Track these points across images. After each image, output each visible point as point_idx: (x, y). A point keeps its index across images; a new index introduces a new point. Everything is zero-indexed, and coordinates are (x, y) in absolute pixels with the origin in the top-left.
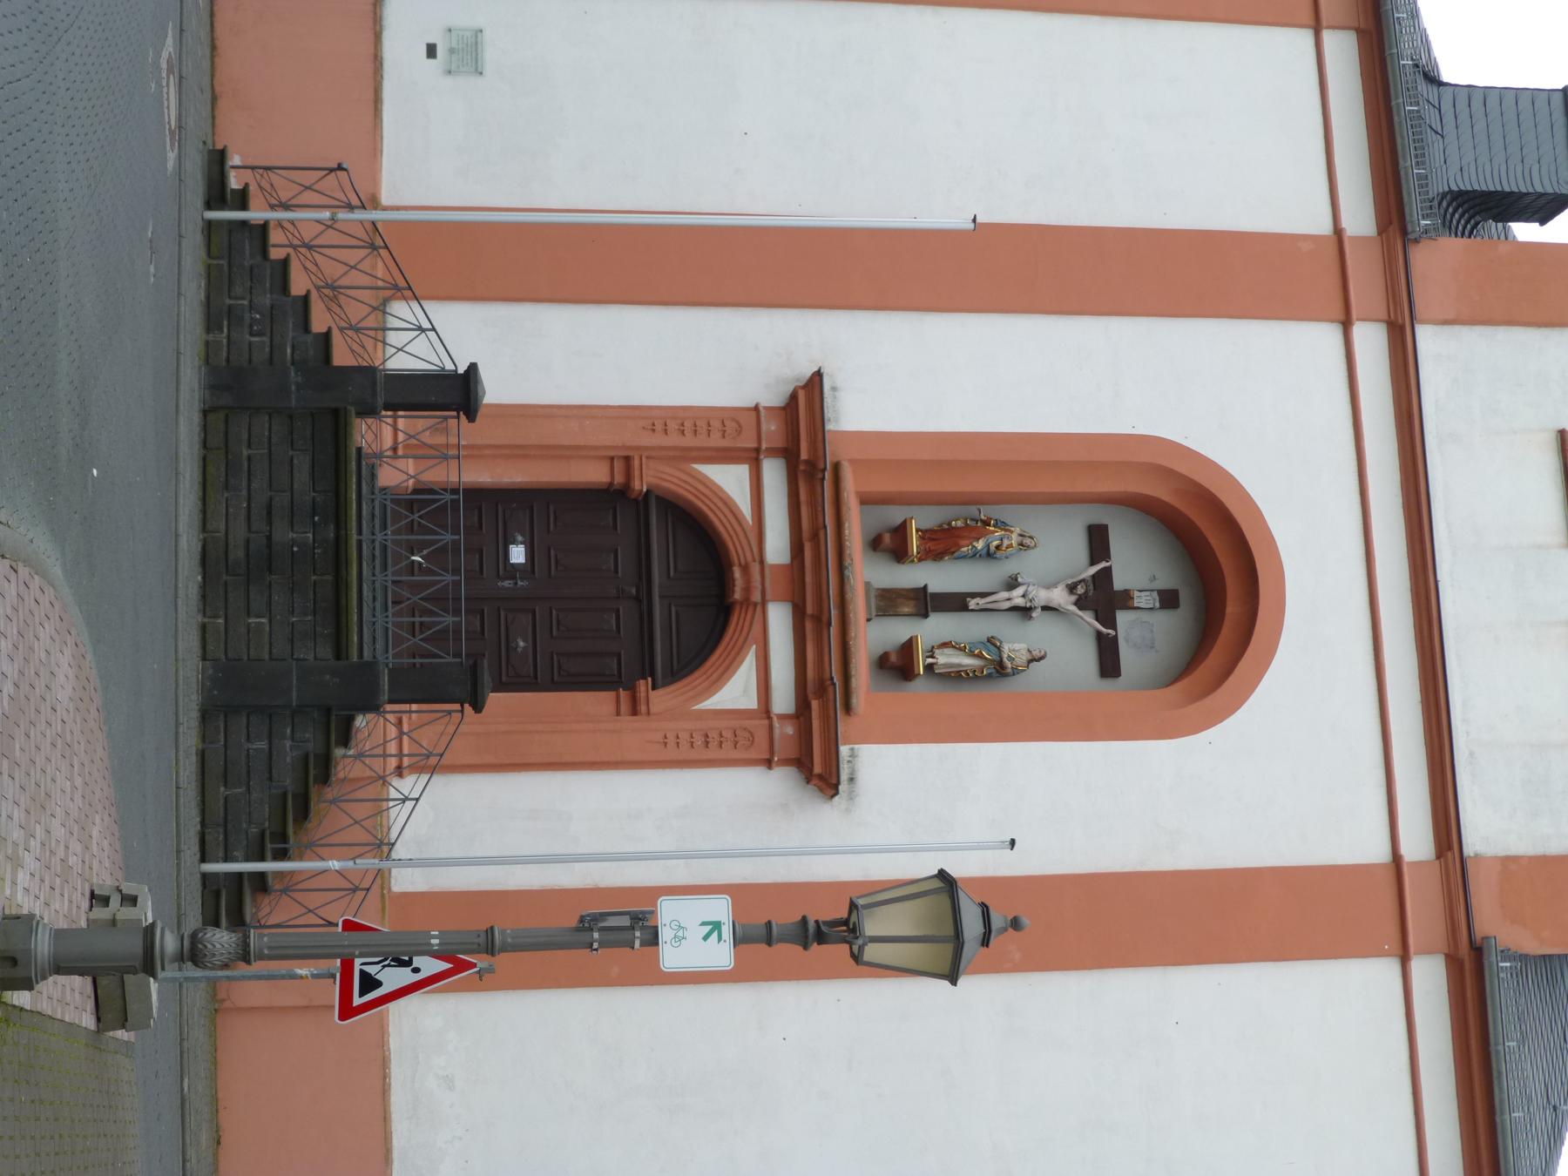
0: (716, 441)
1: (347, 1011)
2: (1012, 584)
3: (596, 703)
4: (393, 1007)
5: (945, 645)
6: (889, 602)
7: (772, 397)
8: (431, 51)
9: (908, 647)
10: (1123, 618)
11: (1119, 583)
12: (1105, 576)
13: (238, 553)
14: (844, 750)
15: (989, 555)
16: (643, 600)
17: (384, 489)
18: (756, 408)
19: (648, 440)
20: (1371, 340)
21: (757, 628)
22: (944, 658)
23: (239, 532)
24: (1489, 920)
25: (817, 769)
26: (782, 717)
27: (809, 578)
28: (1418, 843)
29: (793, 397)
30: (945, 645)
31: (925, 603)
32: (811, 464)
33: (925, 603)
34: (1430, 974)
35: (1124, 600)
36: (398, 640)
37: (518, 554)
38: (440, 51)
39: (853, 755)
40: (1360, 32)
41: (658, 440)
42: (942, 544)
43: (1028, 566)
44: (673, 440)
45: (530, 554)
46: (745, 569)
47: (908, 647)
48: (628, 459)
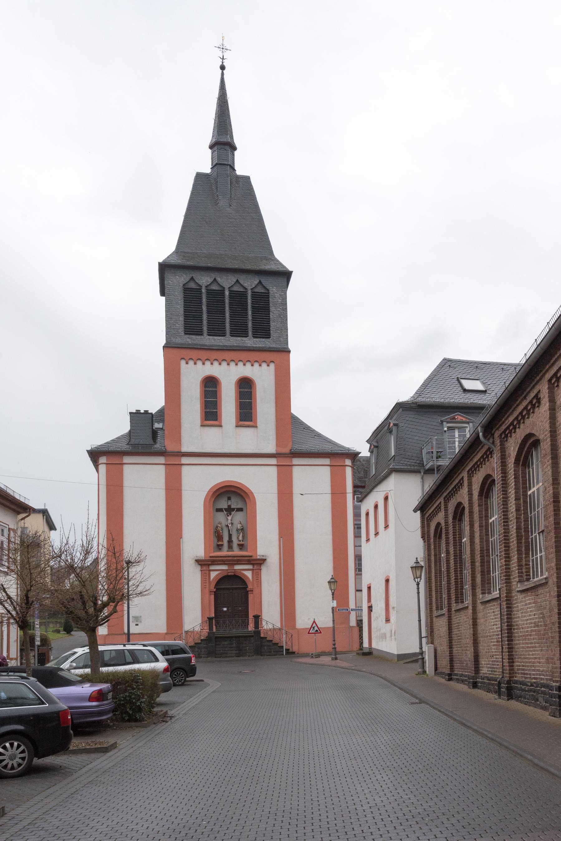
0: (207, 577)
1: (321, 633)
2: (227, 526)
3: (251, 597)
4: (319, 627)
5: (238, 538)
6: (230, 547)
7: (199, 568)
8: (137, 625)
9: (239, 545)
10: (232, 507)
11: (226, 507)
12: (226, 510)
13: (237, 652)
14: (258, 557)
15: (222, 530)
16: (233, 589)
17: (187, 632)
18: (201, 570)
19: (207, 589)
20: (184, 460)
21: (238, 571)
22: (241, 538)
23: (234, 652)
24: (286, 450)
25: (262, 562)
26: (253, 567)
27: (231, 562)
28: (274, 461)
29: (200, 564)
30: (238, 538)
31: (230, 541)
32: (212, 562)
33: (230, 541)
34: (295, 461)
35: (229, 506)
36: (244, 628)
37: (225, 609)
38: (137, 623)
39: (259, 556)
40: (124, 455)
41: (207, 586)
42: (219, 537)
43: (224, 522)
44: (207, 584)
45: (225, 607)
46: (229, 573)
47: (239, 545)
48: (210, 592)
